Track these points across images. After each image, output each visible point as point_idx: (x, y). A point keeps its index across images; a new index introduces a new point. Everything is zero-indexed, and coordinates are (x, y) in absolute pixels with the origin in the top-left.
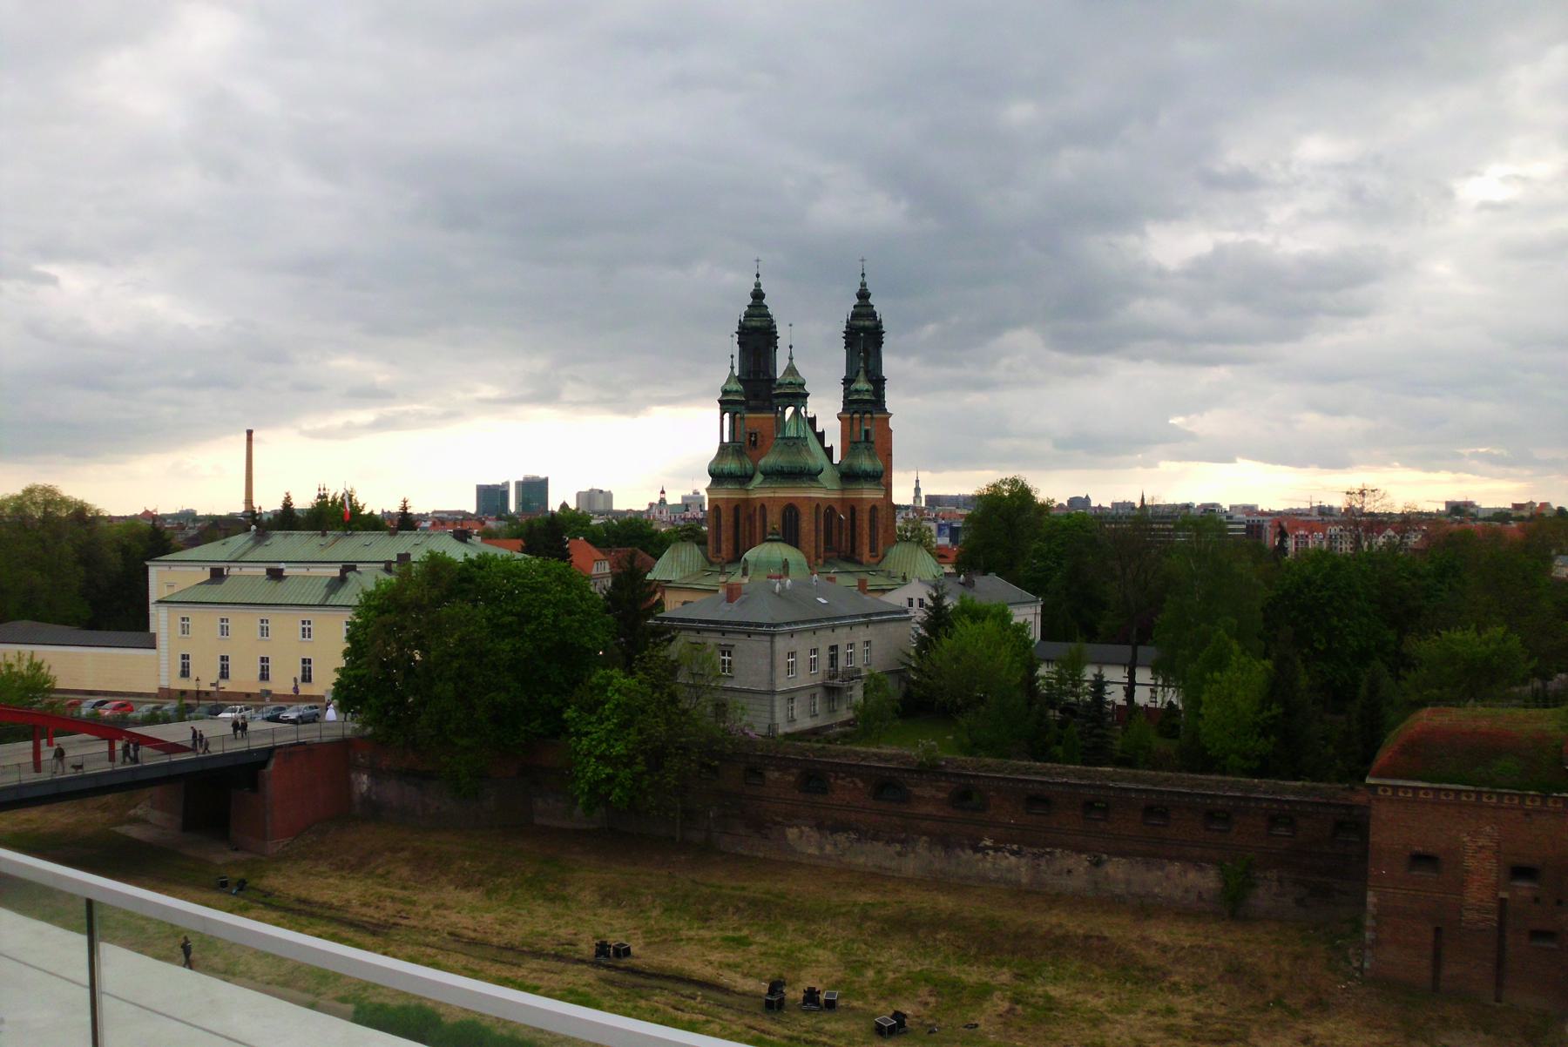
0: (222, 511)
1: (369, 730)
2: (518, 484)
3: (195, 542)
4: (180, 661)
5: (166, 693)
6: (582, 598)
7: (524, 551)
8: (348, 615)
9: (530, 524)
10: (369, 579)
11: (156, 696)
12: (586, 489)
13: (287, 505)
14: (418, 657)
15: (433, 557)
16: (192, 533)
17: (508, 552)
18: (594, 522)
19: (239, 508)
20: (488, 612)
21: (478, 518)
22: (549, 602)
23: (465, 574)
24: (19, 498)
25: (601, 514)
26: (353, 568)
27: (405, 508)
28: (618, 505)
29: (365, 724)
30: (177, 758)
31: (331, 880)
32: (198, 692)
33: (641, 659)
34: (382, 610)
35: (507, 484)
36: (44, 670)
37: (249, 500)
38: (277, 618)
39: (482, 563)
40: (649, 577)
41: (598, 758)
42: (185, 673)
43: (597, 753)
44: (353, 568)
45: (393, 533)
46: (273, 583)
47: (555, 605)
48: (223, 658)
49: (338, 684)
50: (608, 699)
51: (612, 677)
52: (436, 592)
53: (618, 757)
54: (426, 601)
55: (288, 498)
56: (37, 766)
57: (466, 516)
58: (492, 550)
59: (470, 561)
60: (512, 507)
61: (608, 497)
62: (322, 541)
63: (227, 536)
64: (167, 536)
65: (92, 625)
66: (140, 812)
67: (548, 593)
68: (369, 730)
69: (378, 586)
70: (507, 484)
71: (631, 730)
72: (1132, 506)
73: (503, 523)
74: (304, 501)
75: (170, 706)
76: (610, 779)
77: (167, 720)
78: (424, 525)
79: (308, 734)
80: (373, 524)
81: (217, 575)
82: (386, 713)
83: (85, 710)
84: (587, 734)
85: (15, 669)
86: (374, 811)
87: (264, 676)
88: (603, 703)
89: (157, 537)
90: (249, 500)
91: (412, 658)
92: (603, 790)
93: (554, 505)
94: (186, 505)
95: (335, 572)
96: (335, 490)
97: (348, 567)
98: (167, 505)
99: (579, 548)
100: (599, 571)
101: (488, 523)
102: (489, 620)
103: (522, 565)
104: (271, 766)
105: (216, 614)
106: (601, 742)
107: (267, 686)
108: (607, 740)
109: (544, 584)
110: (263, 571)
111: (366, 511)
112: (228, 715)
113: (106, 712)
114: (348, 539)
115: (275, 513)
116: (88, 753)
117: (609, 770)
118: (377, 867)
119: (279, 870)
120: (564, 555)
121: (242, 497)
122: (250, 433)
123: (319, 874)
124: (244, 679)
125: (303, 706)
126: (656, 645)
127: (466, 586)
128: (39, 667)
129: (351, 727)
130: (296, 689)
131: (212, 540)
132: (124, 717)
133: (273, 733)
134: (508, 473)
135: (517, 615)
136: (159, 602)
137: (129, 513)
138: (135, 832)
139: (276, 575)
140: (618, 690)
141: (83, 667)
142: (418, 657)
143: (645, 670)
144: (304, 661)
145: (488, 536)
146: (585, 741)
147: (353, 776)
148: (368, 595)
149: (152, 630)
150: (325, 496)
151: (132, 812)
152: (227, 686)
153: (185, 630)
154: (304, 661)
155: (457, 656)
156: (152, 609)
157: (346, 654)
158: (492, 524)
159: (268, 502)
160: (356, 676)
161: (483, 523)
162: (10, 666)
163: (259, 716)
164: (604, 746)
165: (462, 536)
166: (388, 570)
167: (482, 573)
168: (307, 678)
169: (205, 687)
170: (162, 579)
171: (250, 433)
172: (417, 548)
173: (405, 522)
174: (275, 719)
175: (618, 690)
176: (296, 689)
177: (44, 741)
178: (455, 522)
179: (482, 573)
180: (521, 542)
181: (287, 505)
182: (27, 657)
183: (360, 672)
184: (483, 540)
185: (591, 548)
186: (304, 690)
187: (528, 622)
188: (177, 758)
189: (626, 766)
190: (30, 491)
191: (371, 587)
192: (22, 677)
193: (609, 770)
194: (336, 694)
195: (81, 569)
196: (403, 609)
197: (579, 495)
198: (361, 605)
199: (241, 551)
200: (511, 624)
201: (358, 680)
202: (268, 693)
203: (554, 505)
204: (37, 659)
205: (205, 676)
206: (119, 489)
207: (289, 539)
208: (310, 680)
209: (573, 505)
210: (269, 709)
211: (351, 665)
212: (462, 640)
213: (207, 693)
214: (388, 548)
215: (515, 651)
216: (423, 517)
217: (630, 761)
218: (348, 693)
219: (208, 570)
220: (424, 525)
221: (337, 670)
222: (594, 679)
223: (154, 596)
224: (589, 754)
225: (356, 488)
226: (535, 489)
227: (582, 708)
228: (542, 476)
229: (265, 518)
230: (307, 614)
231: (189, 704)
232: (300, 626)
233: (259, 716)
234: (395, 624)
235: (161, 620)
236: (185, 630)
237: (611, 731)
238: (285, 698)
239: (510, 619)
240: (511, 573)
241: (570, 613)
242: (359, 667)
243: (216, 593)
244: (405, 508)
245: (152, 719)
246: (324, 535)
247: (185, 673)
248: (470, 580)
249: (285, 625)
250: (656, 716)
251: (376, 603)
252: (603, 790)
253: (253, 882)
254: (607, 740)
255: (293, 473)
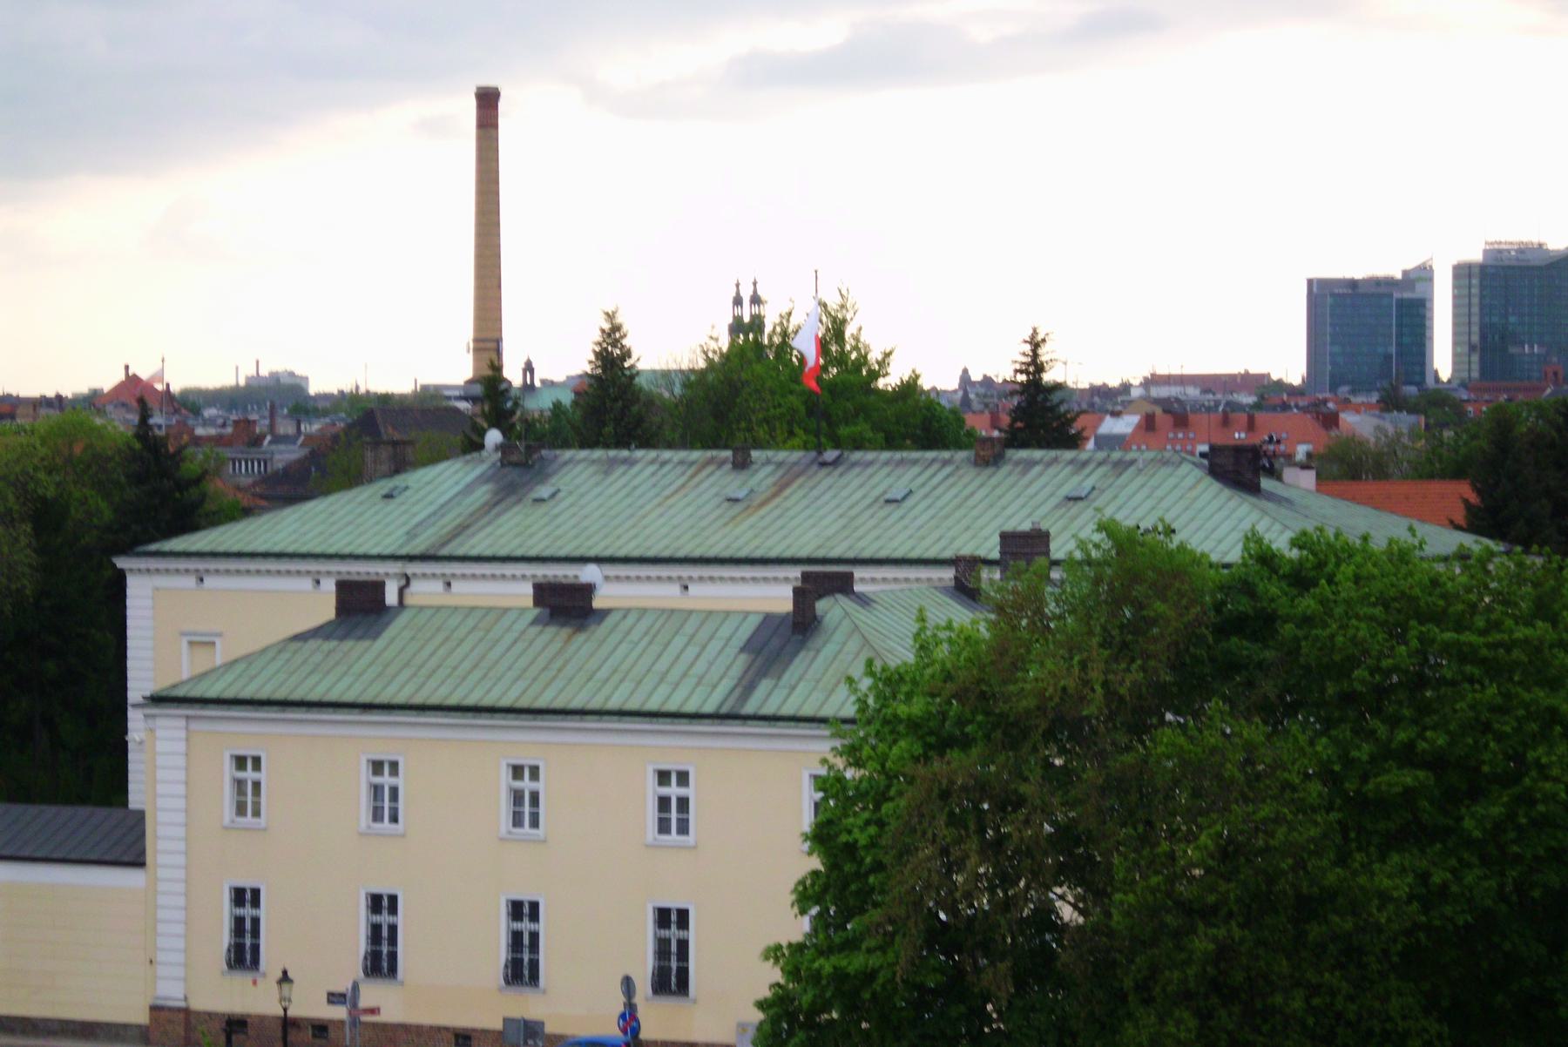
0: (395, 376)
2: (1463, 273)
3: (292, 487)
4: (501, 928)
7: (1479, 522)
8: (815, 754)
9: (1502, 425)
10: (897, 623)
13: (611, 359)
14: (1067, 913)
15: (1125, 543)
16: (285, 456)
17: (1427, 534)
19: (453, 368)
21: (1312, 403)
23: (1244, 605)
26: (842, 584)
27: (1035, 366)
34: (937, 738)
35: (1421, 276)
37: (488, 343)
39: (1315, 567)
44: (842, 584)
45: (989, 456)
46: (554, 636)
52: (1130, 678)
54: (1094, 707)
55: (613, 333)
57: (1268, 393)
59: (1266, 559)
60: (1443, 360)
62: (735, 484)
63: (400, 466)
64: (195, 461)
70: (1421, 276)
72: (863, 360)
78: (1114, 426)
81: (361, 606)
87: (522, 968)
90: (488, 343)
95: (775, 595)
97: (825, 581)
101: (1348, 419)
102: (1327, 775)
105: (349, 748)
109: (1535, 648)
110: (522, 594)
114: (826, 480)
115: (694, 381)
122: (488, 101)
127: (1237, 644)
130: (629, 1018)
135: (1437, 763)
136: (157, 700)
139: (566, 605)
145: (1346, 468)
148: (891, 682)
149: (135, 800)
150: (757, 323)
152: (390, 1003)
153: (247, 799)
155: (1209, 914)
156: (137, 723)
157: (806, 895)
158: (1361, 423)
159: (550, 351)
160: (840, 976)
161: (1330, 421)
165: (1242, 468)
166: (966, 590)
167: (1308, 604)
169: (310, 1004)
170: (174, 618)
171: (488, 101)
173: (1037, 415)
176: (629, 1018)
179: (1308, 604)
180: (1465, 489)
181: (611, 359)
183: (855, 963)
184: (1325, 481)
191: (901, 654)
196: (1012, 733)
200: (1409, 794)
201: (847, 989)
207: (620, 479)
208: (683, 986)
211: (831, 933)
212: (1228, 854)
214: (971, 509)
215: (1429, 896)
216: (1107, 399)
219: (329, 586)
223: (141, 680)
229: (540, 404)
230: (673, 748)
232: (652, 790)
234: (982, 788)
235: (166, 764)
236: (247, 799)
239: (1408, 778)
240: (1410, 602)
242: (850, 945)
243: (359, 668)
244: (1035, 366)
246: (742, 464)
248: (1261, 624)
249: (600, 781)
251: (917, 707)
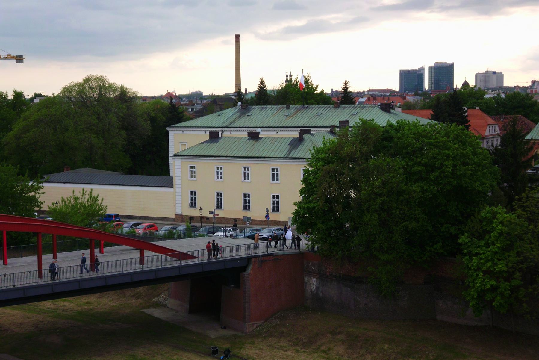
0: (220, 92)
1: (318, 246)
2: (430, 68)
3: (200, 114)
5: (180, 218)
6: (474, 154)
9: (438, 98)
10: (319, 139)
11: (173, 220)
12: (482, 70)
13: (262, 86)
15: (364, 123)
16: (199, 107)
18: (487, 96)
19: (231, 90)
20: (403, 162)
22: (448, 156)
24: (81, 84)
25: (493, 90)
26: (308, 132)
27: (346, 88)
28: (508, 82)
29: (315, 242)
30: (185, 263)
31: (289, 353)
32: (202, 218)
33: (520, 200)
34: (327, 161)
35: (422, 69)
36: (99, 202)
37: (238, 85)
38: (255, 167)
39: (401, 127)
40: (528, 137)
41: (485, 273)
42: (193, 204)
43: (485, 268)
44: (308, 132)
45: (337, 106)
46: (252, 142)
47: (454, 158)
48: (218, 194)
49: (296, 214)
50: (493, 229)
51: (496, 213)
53: (500, 272)
56: (142, 262)
57: (392, 93)
58: (410, 118)
59: (391, 126)
60: (426, 86)
61: (500, 76)
62: (287, 112)
65: (132, 171)
66: (161, 300)
67: (448, 149)
68: (318, 246)
69: (324, 144)
70: (422, 69)
71: (511, 253)
73: (419, 98)
74: (274, 84)
75: (182, 227)
76: (494, 289)
77: (180, 237)
78: (361, 100)
79: (279, 249)
80: (323, 99)
81: (214, 137)
82: (330, 234)
83: (126, 228)
84: (477, 254)
85: (80, 201)
86: (320, 304)
87: (246, 207)
88: (489, 232)
89: (174, 111)
90: (238, 85)
91: (348, 196)
92: (488, 297)
93: (458, 84)
94: (196, 89)
96: (298, 76)
97: (305, 131)
98: (182, 88)
99: (476, 117)
100: (489, 132)
101: (408, 98)
103: (428, 129)
104: (250, 270)
106: (487, 261)
107: (248, 214)
108: (492, 260)
111: (319, 91)
112: (221, 234)
113: (139, 230)
114: (305, 111)
116: (117, 260)
117: (493, 282)
118: (322, 345)
119: (253, 343)
120: (464, 121)
121: (234, 82)
122: (237, 37)
123: (281, 348)
124: (233, 209)
125: (272, 228)
126: (532, 189)
127: (386, 143)
128: (95, 199)
129: (305, 242)
130: (267, 216)
131: (212, 112)
132: (151, 234)
133: (251, 247)
134: (423, 61)
135: (425, 165)
136: (175, 155)
137: (157, 94)
138: (157, 313)
139: (254, 136)
140: (502, 223)
141: (125, 199)
142: (353, 195)
143: (523, 208)
144: (274, 197)
145: (407, 108)
146: (475, 260)
147: (306, 279)
148: (318, 151)
150: (291, 80)
151: (155, 299)
152: (221, 214)
153: (193, 174)
154: (274, 197)
155: (380, 195)
156: (171, 159)
157: (302, 192)
158: (410, 99)
159: (250, 86)
160: (308, 208)
161: (404, 98)
162: (76, 199)
163: (242, 235)
164: (490, 264)
165: (387, 108)
166: (332, 133)
167: (399, 135)
168: (276, 208)
169: (206, 214)
170: (178, 139)
171: (237, 37)
172: (352, 116)
173: (346, 98)
174: (251, 237)
175: (502, 223)
176: (267, 216)
177: (97, 251)
178: (384, 98)
179: (399, 135)
181: (262, 86)
182: (88, 192)
183: (311, 205)
185: (483, 114)
186: (274, 217)
187: (433, 171)
188: (185, 263)
189: (507, 279)
190: (87, 80)
191: (320, 145)
192: (85, 206)
193: (493, 282)
194: (295, 221)
195: (123, 133)
196: (342, 160)
197: (477, 76)
198: (313, 158)
199: (231, 120)
200: (420, 171)
202: (248, 219)
203: (458, 84)
204: (94, 194)
205: (206, 206)
206: (148, 77)
209: (472, 83)
210: (248, 231)
211: (306, 200)
212: (384, 183)
213: (208, 218)
214: (333, 117)
216: (360, 94)
217: (509, 277)
218: (304, 219)
219: (208, 133)
220: (361, 100)
221: (295, 204)
222: (482, 214)
223: (172, 152)
224: (479, 269)
225: (311, 75)
226: (443, 72)
227: (473, 235)
228: (449, 62)
231: (194, 226)
232: (271, 172)
233: (242, 235)
235: (177, 168)
236: (193, 174)
237: (496, 253)
238: (260, 222)
239: (420, 168)
240: (420, 134)
241: (465, 164)
242: (310, 202)
243: (214, 149)
244: (346, 88)
245: (170, 236)
246: (288, 108)
247: (193, 204)
248: (389, 139)
249: (261, 171)
250: (531, 243)
251: (323, 155)
252: (488, 297)
253: (234, 351)
254: (492, 260)
255: (268, 67)
